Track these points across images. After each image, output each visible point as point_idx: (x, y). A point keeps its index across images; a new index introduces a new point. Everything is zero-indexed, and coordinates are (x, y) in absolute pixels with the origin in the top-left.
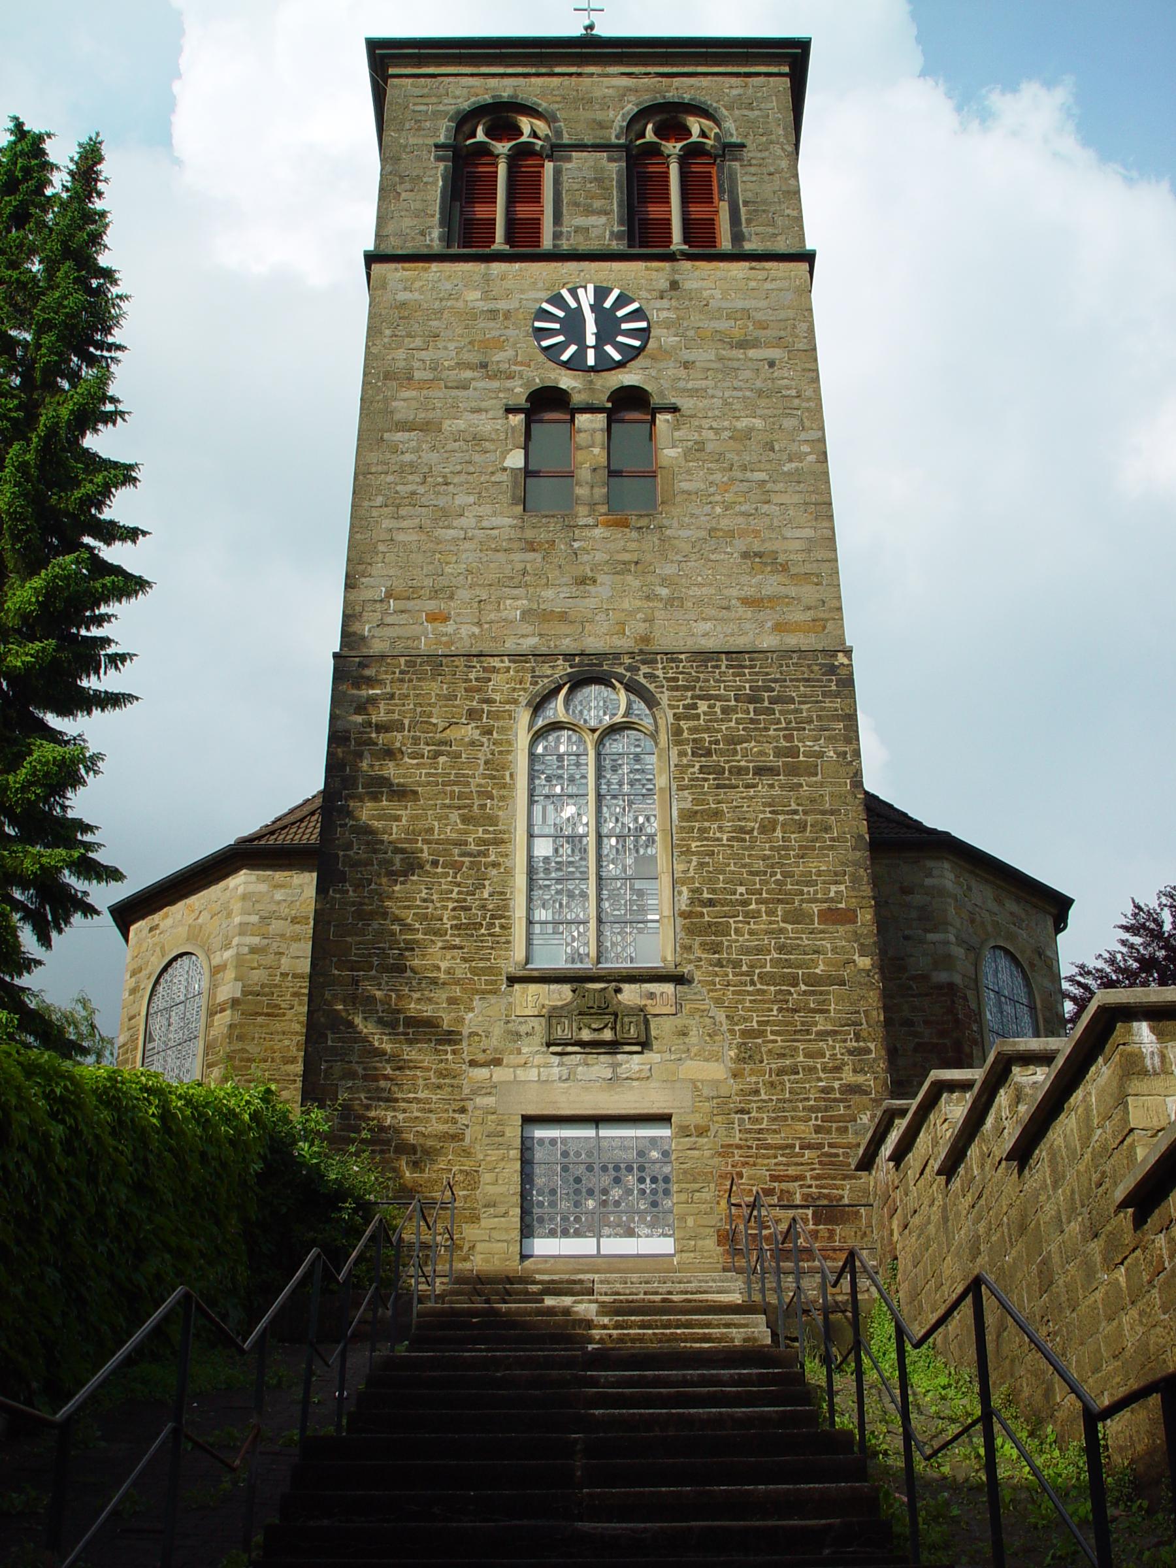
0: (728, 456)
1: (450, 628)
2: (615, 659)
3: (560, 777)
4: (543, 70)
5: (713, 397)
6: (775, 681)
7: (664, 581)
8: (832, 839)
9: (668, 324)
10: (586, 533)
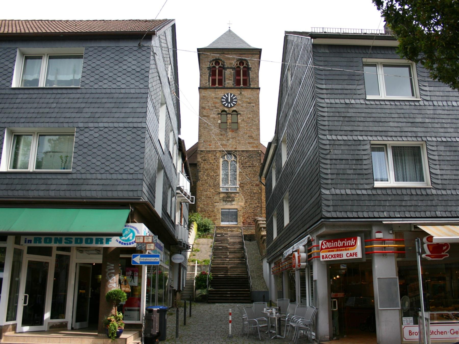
7: (238, 140)
9: (239, 100)
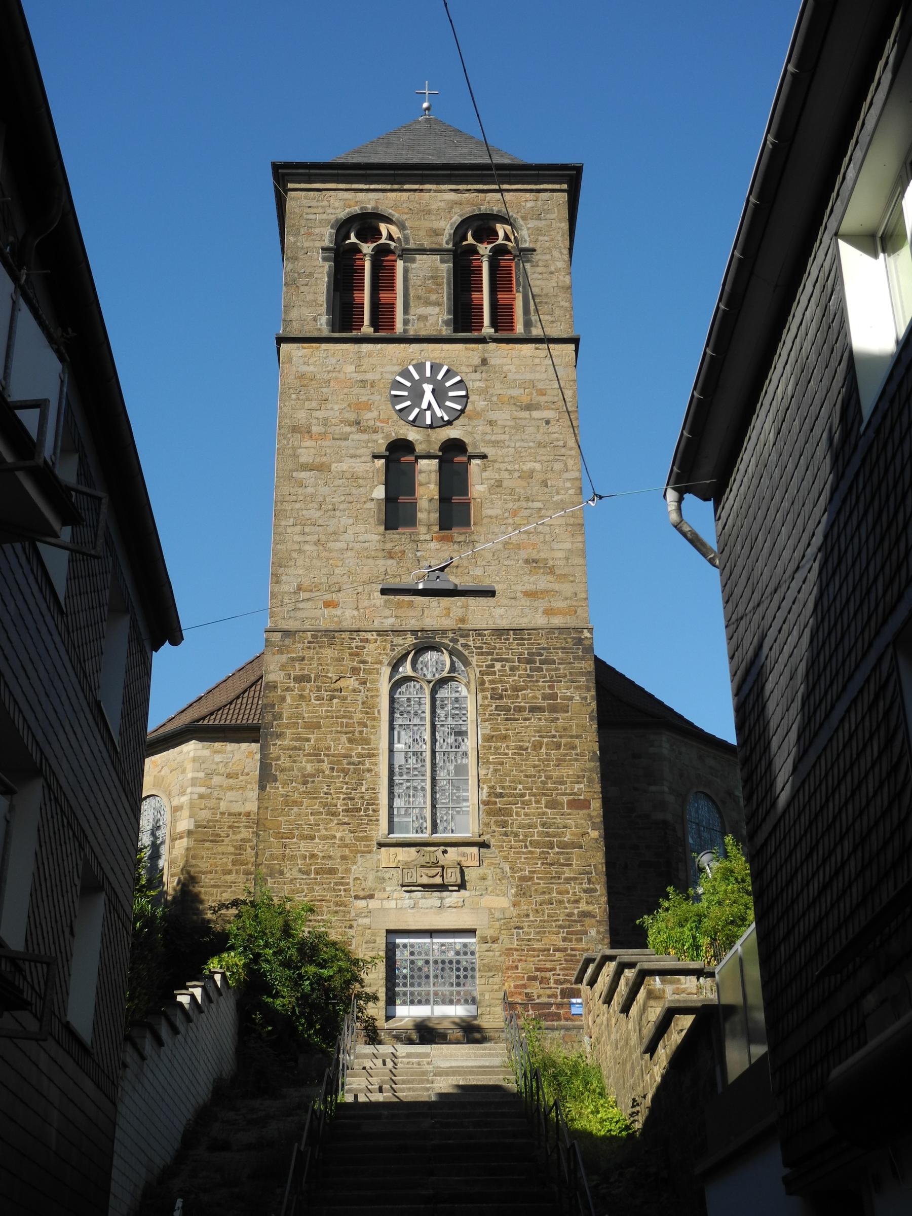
0: (518, 490)
1: (338, 612)
2: (443, 633)
3: (409, 712)
4: (396, 187)
5: (508, 447)
6: (544, 649)
8: (577, 754)
10: (425, 546)
